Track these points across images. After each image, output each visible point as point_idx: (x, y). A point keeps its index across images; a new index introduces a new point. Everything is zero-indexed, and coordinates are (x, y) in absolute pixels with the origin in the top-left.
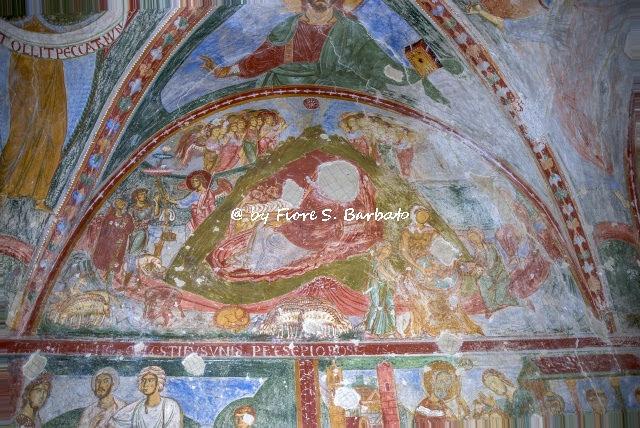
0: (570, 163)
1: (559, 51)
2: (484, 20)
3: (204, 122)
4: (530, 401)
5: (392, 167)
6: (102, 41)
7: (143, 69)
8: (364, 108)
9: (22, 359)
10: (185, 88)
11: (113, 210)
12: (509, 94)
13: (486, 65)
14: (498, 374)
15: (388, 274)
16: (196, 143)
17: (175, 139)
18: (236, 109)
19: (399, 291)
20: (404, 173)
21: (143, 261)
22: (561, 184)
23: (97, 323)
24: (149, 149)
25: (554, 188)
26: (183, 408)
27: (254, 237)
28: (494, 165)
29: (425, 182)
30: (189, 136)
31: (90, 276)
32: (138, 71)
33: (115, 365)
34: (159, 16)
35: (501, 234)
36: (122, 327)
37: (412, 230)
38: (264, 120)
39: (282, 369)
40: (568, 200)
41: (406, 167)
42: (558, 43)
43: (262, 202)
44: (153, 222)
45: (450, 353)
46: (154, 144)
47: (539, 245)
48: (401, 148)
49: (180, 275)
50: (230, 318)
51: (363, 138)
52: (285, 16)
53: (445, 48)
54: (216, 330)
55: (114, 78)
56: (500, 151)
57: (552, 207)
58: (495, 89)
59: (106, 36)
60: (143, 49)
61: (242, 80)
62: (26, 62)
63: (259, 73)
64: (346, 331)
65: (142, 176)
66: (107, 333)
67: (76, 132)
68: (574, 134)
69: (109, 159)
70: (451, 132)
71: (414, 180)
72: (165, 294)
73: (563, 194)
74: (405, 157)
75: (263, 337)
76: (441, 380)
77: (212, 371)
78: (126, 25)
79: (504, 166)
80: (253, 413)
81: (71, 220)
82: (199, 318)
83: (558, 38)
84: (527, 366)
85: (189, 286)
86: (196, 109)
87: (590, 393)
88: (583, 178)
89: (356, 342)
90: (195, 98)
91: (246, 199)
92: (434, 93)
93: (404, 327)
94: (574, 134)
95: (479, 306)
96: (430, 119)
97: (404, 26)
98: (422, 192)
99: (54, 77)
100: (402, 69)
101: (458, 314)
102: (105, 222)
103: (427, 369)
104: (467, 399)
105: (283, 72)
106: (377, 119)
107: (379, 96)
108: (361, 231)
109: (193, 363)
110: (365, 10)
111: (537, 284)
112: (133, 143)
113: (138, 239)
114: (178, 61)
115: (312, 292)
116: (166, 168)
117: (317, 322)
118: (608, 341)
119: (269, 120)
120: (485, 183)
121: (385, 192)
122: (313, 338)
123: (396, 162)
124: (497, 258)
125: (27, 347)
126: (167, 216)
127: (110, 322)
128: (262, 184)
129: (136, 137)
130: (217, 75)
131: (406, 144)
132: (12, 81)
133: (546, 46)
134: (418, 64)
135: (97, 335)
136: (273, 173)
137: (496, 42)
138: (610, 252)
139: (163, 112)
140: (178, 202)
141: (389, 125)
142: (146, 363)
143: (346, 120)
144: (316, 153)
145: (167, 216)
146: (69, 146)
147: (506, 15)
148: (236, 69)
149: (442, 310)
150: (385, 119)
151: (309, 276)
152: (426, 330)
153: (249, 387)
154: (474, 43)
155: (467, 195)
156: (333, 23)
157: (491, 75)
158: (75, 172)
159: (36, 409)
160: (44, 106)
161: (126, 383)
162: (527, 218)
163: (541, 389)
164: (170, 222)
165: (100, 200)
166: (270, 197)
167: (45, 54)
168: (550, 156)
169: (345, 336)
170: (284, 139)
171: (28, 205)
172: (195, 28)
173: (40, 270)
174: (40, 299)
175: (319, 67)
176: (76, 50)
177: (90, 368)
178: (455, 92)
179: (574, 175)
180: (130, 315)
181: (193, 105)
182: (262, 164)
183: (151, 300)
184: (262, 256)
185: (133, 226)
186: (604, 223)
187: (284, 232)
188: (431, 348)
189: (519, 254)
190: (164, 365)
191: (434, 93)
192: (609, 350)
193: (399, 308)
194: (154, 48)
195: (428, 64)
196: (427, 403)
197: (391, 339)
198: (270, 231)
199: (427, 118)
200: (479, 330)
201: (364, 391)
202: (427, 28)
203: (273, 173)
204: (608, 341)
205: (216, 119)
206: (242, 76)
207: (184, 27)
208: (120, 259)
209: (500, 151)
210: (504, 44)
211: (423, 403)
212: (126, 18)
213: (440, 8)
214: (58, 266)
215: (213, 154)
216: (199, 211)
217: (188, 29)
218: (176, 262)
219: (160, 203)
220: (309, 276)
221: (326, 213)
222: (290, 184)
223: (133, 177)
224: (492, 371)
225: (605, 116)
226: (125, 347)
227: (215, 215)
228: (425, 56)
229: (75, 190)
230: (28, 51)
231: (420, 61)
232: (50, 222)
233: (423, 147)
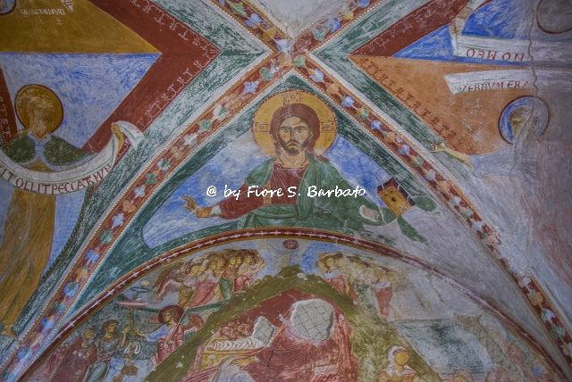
1: (530, 183)
2: (450, 157)
3: (186, 259)
5: (370, 307)
6: (93, 179)
7: (128, 206)
8: (343, 249)
10: (166, 225)
11: (80, 340)
12: (485, 227)
13: (457, 200)
16: (175, 279)
20: (382, 312)
22: (555, 320)
24: (129, 282)
25: (548, 325)
27: (218, 375)
28: (479, 303)
29: (405, 322)
32: (122, 207)
34: (144, 158)
37: (390, 372)
38: (243, 259)
42: (528, 176)
43: (231, 339)
44: (117, 353)
46: (134, 278)
48: (379, 287)
51: (341, 277)
52: (261, 159)
53: (416, 186)
55: (99, 212)
56: (484, 287)
57: (551, 348)
58: (470, 223)
59: (96, 174)
60: (128, 187)
61: (225, 221)
62: (26, 197)
63: (240, 214)
65: (117, 307)
67: (57, 261)
68: (561, 267)
69: (84, 288)
70: (432, 271)
71: (393, 319)
74: (384, 296)
78: (114, 166)
79: (490, 304)
81: (34, 347)
83: (528, 171)
86: (180, 247)
90: (177, 236)
91: (215, 335)
94: (561, 267)
96: (410, 259)
97: (375, 168)
99: (46, 209)
100: (376, 208)
102: (68, 353)
105: (263, 214)
106: (355, 259)
107: (357, 236)
108: (334, 373)
110: (335, 152)
112: (112, 275)
113: (98, 372)
114: (161, 199)
116: (140, 302)
119: (248, 259)
120: (468, 323)
121: (361, 332)
123: (374, 300)
126: (132, 349)
128: (235, 321)
129: (115, 269)
130: (199, 216)
131: (385, 283)
132: (10, 212)
133: (516, 179)
134: (392, 203)
136: (246, 309)
137: (465, 177)
139: (145, 248)
140: (146, 335)
141: (367, 265)
143: (324, 261)
144: (292, 291)
145: (132, 349)
146: (48, 274)
147: (471, 151)
148: (217, 210)
150: (363, 259)
154: (443, 179)
155: (451, 335)
156: (307, 165)
157: (463, 209)
158: (49, 299)
160: (32, 237)
164: (134, 355)
165: (71, 329)
166: (241, 334)
168: (537, 290)
170: (260, 277)
172: (176, 170)
175: (297, 210)
176: (69, 188)
178: (431, 229)
181: (176, 242)
182: (236, 301)
185: (96, 358)
187: (251, 372)
191: (410, 232)
194: (138, 186)
195: (401, 203)
198: (236, 369)
199: (406, 257)
202: (396, 167)
203: (246, 309)
206: (223, 217)
207: (166, 168)
209: (484, 287)
210: (473, 178)
212: (114, 159)
213: (406, 147)
215: (189, 290)
216: (166, 346)
217: (170, 170)
219: (128, 334)
221: (292, 194)
223: (108, 308)
227: (182, 350)
228: (397, 195)
229: (45, 316)
230: (29, 187)
231: (393, 200)
232: (11, 349)
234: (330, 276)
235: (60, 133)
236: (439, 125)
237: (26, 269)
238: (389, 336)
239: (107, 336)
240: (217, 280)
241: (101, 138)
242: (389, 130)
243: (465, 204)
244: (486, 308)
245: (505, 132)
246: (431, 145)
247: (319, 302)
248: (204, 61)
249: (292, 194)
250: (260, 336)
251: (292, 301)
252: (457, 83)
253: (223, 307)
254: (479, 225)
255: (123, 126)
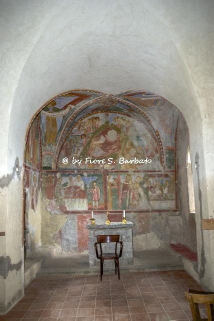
11: (67, 144)
44: (75, 146)
48: (127, 126)
55: (66, 120)
74: (127, 129)
119: (98, 120)
120: (145, 135)
123: (125, 130)
136: (98, 134)
144: (108, 128)
147: (147, 107)
150: (124, 118)
155: (140, 138)
170: (101, 125)
182: (96, 132)
198: (98, 148)
203: (98, 134)
221: (110, 162)
238: (127, 139)
247: (114, 131)
249: (110, 162)
250: (102, 140)
251: (108, 131)
253: (94, 133)
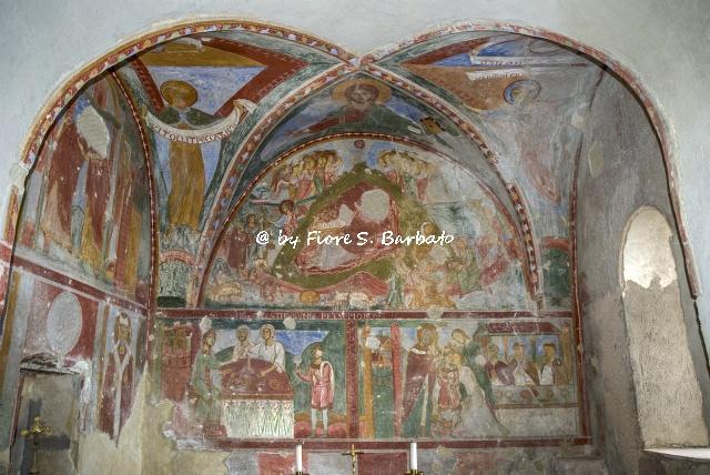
0: (531, 199)
2: (469, 111)
3: (288, 162)
4: (478, 348)
5: (412, 193)
9: (198, 320)
11: (236, 230)
13: (473, 135)
14: (461, 332)
15: (402, 270)
17: (270, 176)
18: (309, 151)
19: (408, 281)
21: (257, 263)
22: (522, 211)
23: (235, 300)
24: (254, 185)
26: (285, 347)
30: (278, 173)
31: (228, 272)
33: (247, 324)
35: (479, 243)
36: (249, 302)
39: (337, 327)
40: (526, 222)
41: (422, 192)
45: (434, 319)
47: (504, 250)
48: (420, 178)
49: (279, 271)
50: (308, 297)
54: (301, 304)
55: (232, 153)
60: (249, 136)
64: (374, 305)
65: (251, 205)
66: (241, 307)
67: (211, 186)
72: (271, 283)
73: (523, 218)
74: (422, 185)
75: (327, 308)
76: (427, 334)
77: (299, 327)
80: (322, 350)
82: (291, 297)
84: (481, 327)
85: (285, 278)
87: (516, 345)
88: (538, 207)
89: (379, 311)
91: (316, 219)
92: (443, 143)
93: (408, 303)
95: (457, 291)
98: (430, 212)
101: (443, 296)
103: (420, 327)
104: (441, 346)
106: (405, 155)
109: (289, 322)
111: (498, 276)
115: (356, 282)
117: (358, 299)
118: (536, 314)
119: (331, 158)
120: (475, 204)
122: (355, 309)
123: (414, 188)
124: (474, 259)
125: (199, 314)
127: (242, 300)
128: (327, 208)
131: (424, 174)
135: (236, 307)
136: (333, 200)
137: (479, 122)
138: (548, 257)
141: (413, 159)
142: (264, 322)
144: (362, 184)
146: (208, 194)
147: (484, 108)
149: (433, 292)
151: (354, 271)
152: (422, 304)
153: (320, 336)
159: (210, 346)
160: (191, 170)
161: (254, 334)
162: (500, 230)
163: (486, 341)
167: (190, 141)
169: (374, 308)
170: (340, 173)
171: (187, 231)
173: (200, 270)
174: (202, 286)
177: (234, 326)
179: (532, 205)
180: (253, 296)
182: (326, 193)
183: (264, 287)
184: (327, 258)
186: (549, 237)
188: (424, 315)
189: (489, 256)
190: (273, 323)
192: (535, 320)
193: (407, 291)
195: (436, 129)
196: (417, 347)
197: (400, 310)
200: (454, 306)
201: (382, 339)
203: (333, 200)
204: (536, 314)
205: (295, 159)
208: (244, 262)
211: (415, 347)
214: (208, 267)
218: (276, 262)
220: (354, 271)
221: (362, 236)
222: (344, 208)
223: (245, 205)
224: (458, 330)
225: (558, 165)
226: (251, 314)
233: (436, 176)
234: (386, 170)
235: (196, 106)
236: (462, 95)
237: (192, 192)
239: (251, 225)
240: (312, 178)
241: (228, 108)
242: (426, 96)
243: (477, 137)
244: (487, 193)
245: (509, 98)
246: (456, 104)
247: (380, 191)
248: (297, 69)
251: (362, 192)
252: (473, 76)
254: (485, 151)
255: (242, 102)
